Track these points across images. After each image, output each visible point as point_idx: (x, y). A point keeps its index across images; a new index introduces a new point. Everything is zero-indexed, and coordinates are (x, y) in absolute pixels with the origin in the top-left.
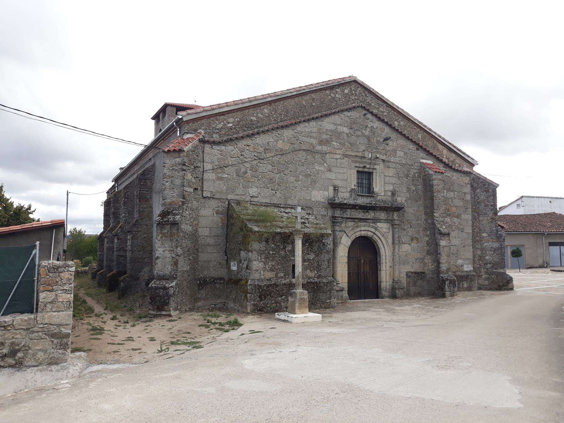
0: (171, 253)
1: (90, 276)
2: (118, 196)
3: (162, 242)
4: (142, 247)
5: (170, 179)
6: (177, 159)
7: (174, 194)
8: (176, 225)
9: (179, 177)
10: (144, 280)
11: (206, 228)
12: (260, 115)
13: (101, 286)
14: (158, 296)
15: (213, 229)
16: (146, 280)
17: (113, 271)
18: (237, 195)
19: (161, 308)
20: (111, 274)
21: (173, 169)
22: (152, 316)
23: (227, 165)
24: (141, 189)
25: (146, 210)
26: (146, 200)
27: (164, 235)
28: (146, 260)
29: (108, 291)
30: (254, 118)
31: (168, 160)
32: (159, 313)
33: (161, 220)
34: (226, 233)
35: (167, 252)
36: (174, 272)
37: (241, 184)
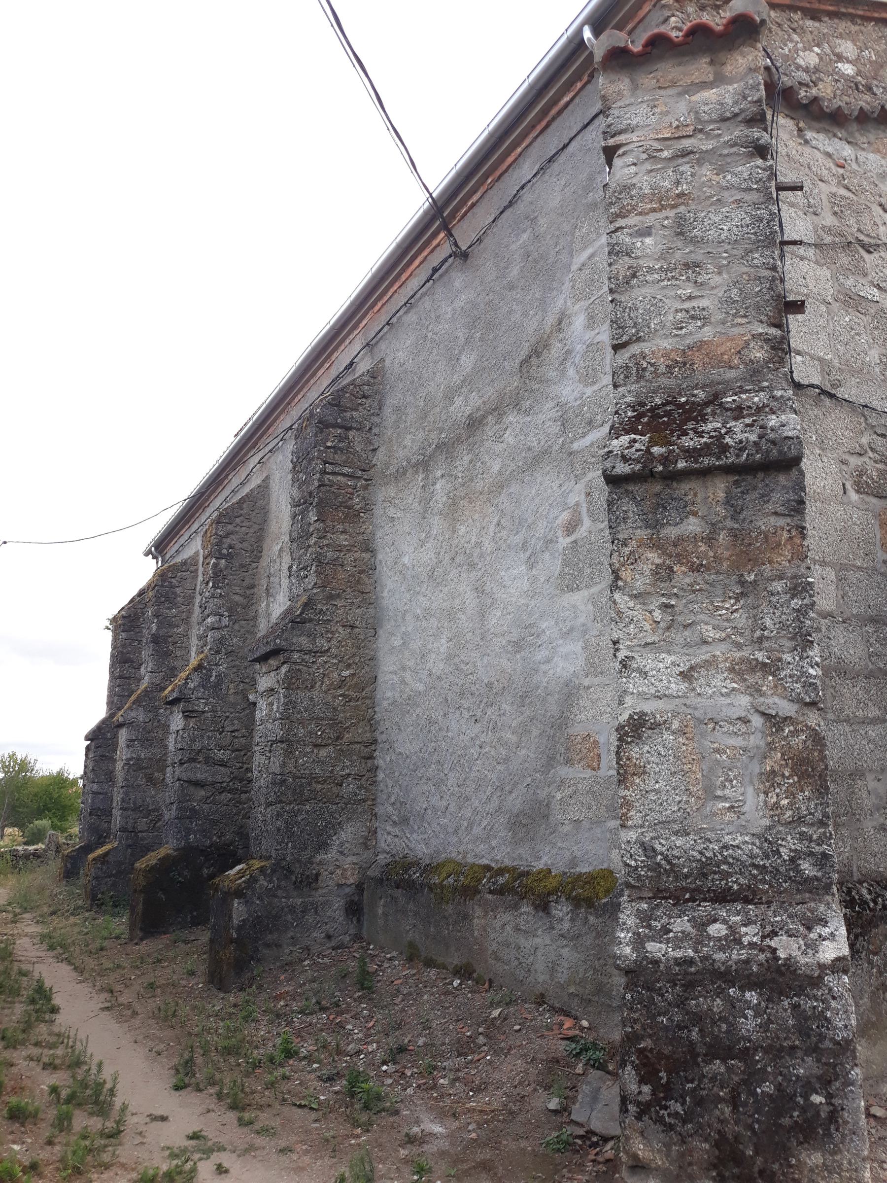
0: (757, 691)
1: (55, 866)
3: (666, 606)
4: (331, 726)
5: (665, 213)
6: (711, 94)
7: (704, 303)
8: (782, 479)
9: (726, 194)
10: (339, 886)
13: (100, 906)
15: (853, 576)
16: (347, 890)
17: (160, 845)
19: (759, 1161)
20: (152, 859)
21: (685, 153)
23: (873, 241)
24: (329, 468)
25: (349, 558)
27: (680, 558)
28: (349, 787)
31: (643, 109)
33: (656, 450)
35: (720, 681)
36: (803, 836)
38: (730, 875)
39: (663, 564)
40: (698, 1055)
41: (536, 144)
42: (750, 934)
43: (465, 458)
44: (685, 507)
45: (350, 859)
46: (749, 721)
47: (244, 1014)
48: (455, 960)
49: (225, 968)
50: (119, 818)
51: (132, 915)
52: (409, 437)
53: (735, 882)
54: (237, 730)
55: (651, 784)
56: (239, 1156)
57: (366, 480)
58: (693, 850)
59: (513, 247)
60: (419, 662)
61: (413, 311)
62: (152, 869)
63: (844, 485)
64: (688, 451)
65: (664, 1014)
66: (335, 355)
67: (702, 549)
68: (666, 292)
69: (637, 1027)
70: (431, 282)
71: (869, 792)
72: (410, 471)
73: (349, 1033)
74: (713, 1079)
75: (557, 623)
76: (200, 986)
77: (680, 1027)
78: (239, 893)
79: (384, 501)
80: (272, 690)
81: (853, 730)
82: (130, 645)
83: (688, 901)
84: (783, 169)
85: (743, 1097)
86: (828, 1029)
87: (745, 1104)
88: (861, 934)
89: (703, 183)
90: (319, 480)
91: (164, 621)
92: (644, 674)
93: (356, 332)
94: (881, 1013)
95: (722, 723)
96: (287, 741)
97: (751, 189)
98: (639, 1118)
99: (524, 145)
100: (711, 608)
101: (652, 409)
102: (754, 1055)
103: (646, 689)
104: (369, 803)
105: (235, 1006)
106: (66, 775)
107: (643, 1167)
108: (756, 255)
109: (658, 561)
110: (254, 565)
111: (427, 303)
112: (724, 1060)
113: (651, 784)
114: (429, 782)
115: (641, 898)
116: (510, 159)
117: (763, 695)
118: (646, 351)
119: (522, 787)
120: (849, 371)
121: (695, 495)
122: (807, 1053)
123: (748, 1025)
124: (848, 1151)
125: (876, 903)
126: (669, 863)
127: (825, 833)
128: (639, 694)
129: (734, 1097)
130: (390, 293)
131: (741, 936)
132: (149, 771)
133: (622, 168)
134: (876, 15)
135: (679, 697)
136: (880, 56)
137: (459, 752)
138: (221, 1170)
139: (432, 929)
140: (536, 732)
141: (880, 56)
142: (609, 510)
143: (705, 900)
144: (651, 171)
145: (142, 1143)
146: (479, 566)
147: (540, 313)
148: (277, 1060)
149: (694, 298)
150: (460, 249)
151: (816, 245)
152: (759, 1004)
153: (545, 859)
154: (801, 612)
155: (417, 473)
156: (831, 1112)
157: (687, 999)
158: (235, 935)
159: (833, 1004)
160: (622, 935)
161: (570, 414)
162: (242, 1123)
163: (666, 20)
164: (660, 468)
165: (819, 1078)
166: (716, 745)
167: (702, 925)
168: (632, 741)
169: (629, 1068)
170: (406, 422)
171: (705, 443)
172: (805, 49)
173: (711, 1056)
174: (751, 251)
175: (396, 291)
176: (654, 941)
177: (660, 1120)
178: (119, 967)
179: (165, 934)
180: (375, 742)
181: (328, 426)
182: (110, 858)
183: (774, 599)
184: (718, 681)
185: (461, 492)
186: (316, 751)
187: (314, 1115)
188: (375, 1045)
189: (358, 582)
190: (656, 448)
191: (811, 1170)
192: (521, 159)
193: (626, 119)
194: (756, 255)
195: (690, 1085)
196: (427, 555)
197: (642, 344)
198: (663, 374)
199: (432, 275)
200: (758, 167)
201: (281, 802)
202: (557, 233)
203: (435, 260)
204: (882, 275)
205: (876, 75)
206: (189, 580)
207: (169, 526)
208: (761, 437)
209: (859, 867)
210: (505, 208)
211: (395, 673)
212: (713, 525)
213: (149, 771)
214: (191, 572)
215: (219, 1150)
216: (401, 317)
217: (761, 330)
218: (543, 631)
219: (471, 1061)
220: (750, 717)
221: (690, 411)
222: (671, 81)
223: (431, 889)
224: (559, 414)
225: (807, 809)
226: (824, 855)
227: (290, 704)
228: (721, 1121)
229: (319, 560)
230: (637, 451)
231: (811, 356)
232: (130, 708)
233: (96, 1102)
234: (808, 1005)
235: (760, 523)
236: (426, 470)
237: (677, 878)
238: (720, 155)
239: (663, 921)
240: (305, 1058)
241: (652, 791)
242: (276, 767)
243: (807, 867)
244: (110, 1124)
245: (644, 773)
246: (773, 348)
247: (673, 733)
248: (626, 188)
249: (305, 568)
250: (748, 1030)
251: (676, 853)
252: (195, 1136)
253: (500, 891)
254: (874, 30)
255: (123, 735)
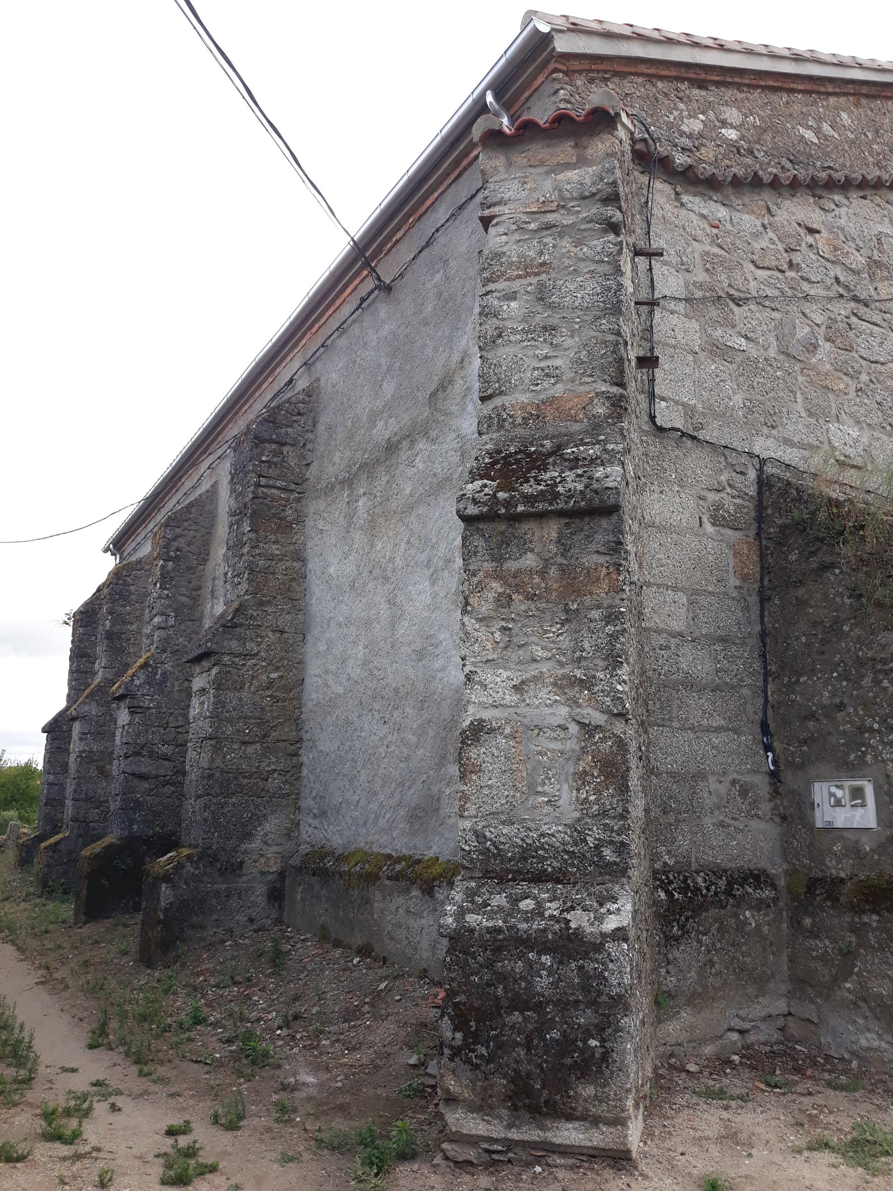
0: (574, 702)
2: (128, 579)
4: (258, 725)
6: (573, 175)
7: (558, 362)
8: (604, 523)
9: (582, 265)
10: (262, 873)
11: (675, 589)
12: (826, 128)
14: (520, 1003)
15: (703, 600)
18: (788, 442)
19: (545, 1093)
20: (97, 847)
21: (548, 227)
22: (471, 1154)
23: (742, 295)
24: (263, 481)
25: (281, 566)
26: (279, 527)
27: (518, 588)
28: (274, 783)
29: (83, 918)
30: (809, 135)
31: (515, 185)
32: (532, 1134)
33: (501, 495)
34: (758, 628)
35: (544, 694)
37: (798, 395)
38: (546, 859)
39: (504, 593)
40: (502, 1008)
41: (450, 191)
42: (553, 908)
43: (383, 479)
44: (525, 544)
45: (274, 849)
46: (567, 728)
47: (165, 987)
48: (358, 940)
49: (153, 947)
50: (71, 808)
51: (77, 900)
52: (338, 454)
53: (549, 865)
54: (181, 726)
55: (485, 781)
56: (133, 1099)
57: (299, 493)
58: (516, 837)
59: (429, 285)
60: (339, 666)
61: (345, 336)
62: (97, 856)
63: (700, 518)
64: (526, 497)
65: (476, 974)
66: (278, 370)
67: (536, 581)
68: (526, 351)
69: (454, 984)
70: (360, 310)
71: (710, 792)
72: (338, 487)
73: (255, 1004)
74: (513, 1027)
75: (452, 636)
76: (131, 964)
77: (489, 985)
78: (166, 878)
79: (314, 514)
80: (204, 690)
81: (698, 738)
82: (88, 640)
83: (510, 880)
84: (658, 231)
85: (535, 1042)
86: (605, 986)
87: (537, 1047)
88: (692, 917)
89: (563, 254)
90: (253, 493)
91: (119, 619)
92: (484, 687)
93: (296, 351)
94: (707, 985)
95: (545, 730)
96: (216, 738)
97: (603, 262)
98: (451, 1059)
99: (440, 191)
100: (541, 631)
101: (504, 458)
102: (546, 1007)
103: (485, 700)
104: (293, 797)
105: (159, 981)
106: (34, 766)
107: (454, 1100)
108: (604, 321)
109: (500, 590)
110: (201, 567)
111: (356, 330)
112: (522, 1012)
113: (485, 781)
114: (345, 778)
115: (472, 878)
116: (428, 203)
117: (579, 706)
118: (507, 404)
119: (419, 783)
120: (712, 415)
121: (533, 535)
122: (589, 1005)
123: (542, 983)
124: (615, 1084)
125: (708, 890)
126: (497, 848)
127: (624, 825)
128: (480, 703)
129: (528, 1042)
130: (326, 317)
131: (545, 910)
132: (101, 763)
133: (495, 236)
134: (762, 83)
135: (512, 706)
136: (764, 121)
137: (370, 751)
138: (114, 1108)
139: (341, 913)
140: (431, 734)
141: (764, 121)
142: (463, 544)
143: (524, 880)
144: (519, 241)
145: (51, 1088)
146: (392, 580)
147: (447, 350)
148: (186, 1026)
149: (549, 357)
150: (384, 282)
151: (686, 300)
152: (552, 965)
153: (435, 848)
154: (613, 637)
155: (343, 490)
156: (603, 1053)
157: (495, 961)
158: (162, 917)
159: (611, 965)
160: (449, 908)
161: (468, 446)
162: (141, 1074)
163: (556, 92)
164: (503, 511)
165: (596, 1026)
166: (539, 748)
167: (515, 901)
168: (472, 744)
169: (446, 1018)
170: (336, 440)
171: (541, 490)
172: (690, 116)
173: (511, 1009)
174: (599, 318)
175: (331, 315)
176: (473, 913)
177: (469, 1061)
178: (59, 947)
179: (107, 918)
180: (300, 740)
181: (263, 441)
182: (62, 847)
183: (592, 625)
184: (543, 694)
185: (378, 510)
186: (243, 748)
187: (206, 1068)
188: (274, 1013)
189: (289, 590)
190: (500, 493)
191: (585, 1100)
192: (437, 204)
193: (500, 193)
194: (604, 321)
195: (494, 1032)
196: (349, 568)
197: (504, 397)
198: (520, 425)
199: (361, 304)
200: (609, 242)
201: (208, 794)
202: (464, 277)
203: (364, 290)
204: (750, 326)
205: (759, 139)
206: (142, 579)
207: (127, 524)
208: (586, 487)
209: (697, 858)
210: (423, 248)
211: (320, 676)
212: (546, 560)
213: (101, 763)
214: (146, 571)
215: (116, 1095)
216: (334, 340)
217: (603, 389)
218: (441, 642)
219: (354, 1026)
220: (568, 725)
221: (536, 460)
222: (540, 161)
223: (341, 876)
224: (460, 445)
225: (611, 804)
226: (623, 844)
227: (219, 703)
228: (517, 1062)
229: (251, 569)
230: (485, 495)
231: (675, 402)
232: (83, 702)
233: (15, 1057)
234: (590, 966)
235: (584, 560)
236: (351, 488)
237: (502, 861)
238: (579, 229)
239: (484, 897)
240: (211, 1024)
241: (486, 786)
242: (204, 763)
243: (608, 853)
244: (23, 1073)
245: (480, 771)
246: (613, 405)
247: (506, 737)
248: (498, 255)
249: (238, 575)
250: (542, 987)
251: (502, 840)
252: (97, 1084)
253: (396, 878)
254: (760, 97)
255: (77, 727)
